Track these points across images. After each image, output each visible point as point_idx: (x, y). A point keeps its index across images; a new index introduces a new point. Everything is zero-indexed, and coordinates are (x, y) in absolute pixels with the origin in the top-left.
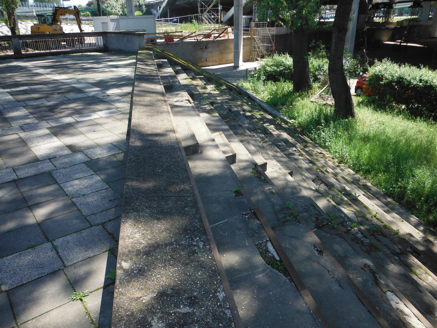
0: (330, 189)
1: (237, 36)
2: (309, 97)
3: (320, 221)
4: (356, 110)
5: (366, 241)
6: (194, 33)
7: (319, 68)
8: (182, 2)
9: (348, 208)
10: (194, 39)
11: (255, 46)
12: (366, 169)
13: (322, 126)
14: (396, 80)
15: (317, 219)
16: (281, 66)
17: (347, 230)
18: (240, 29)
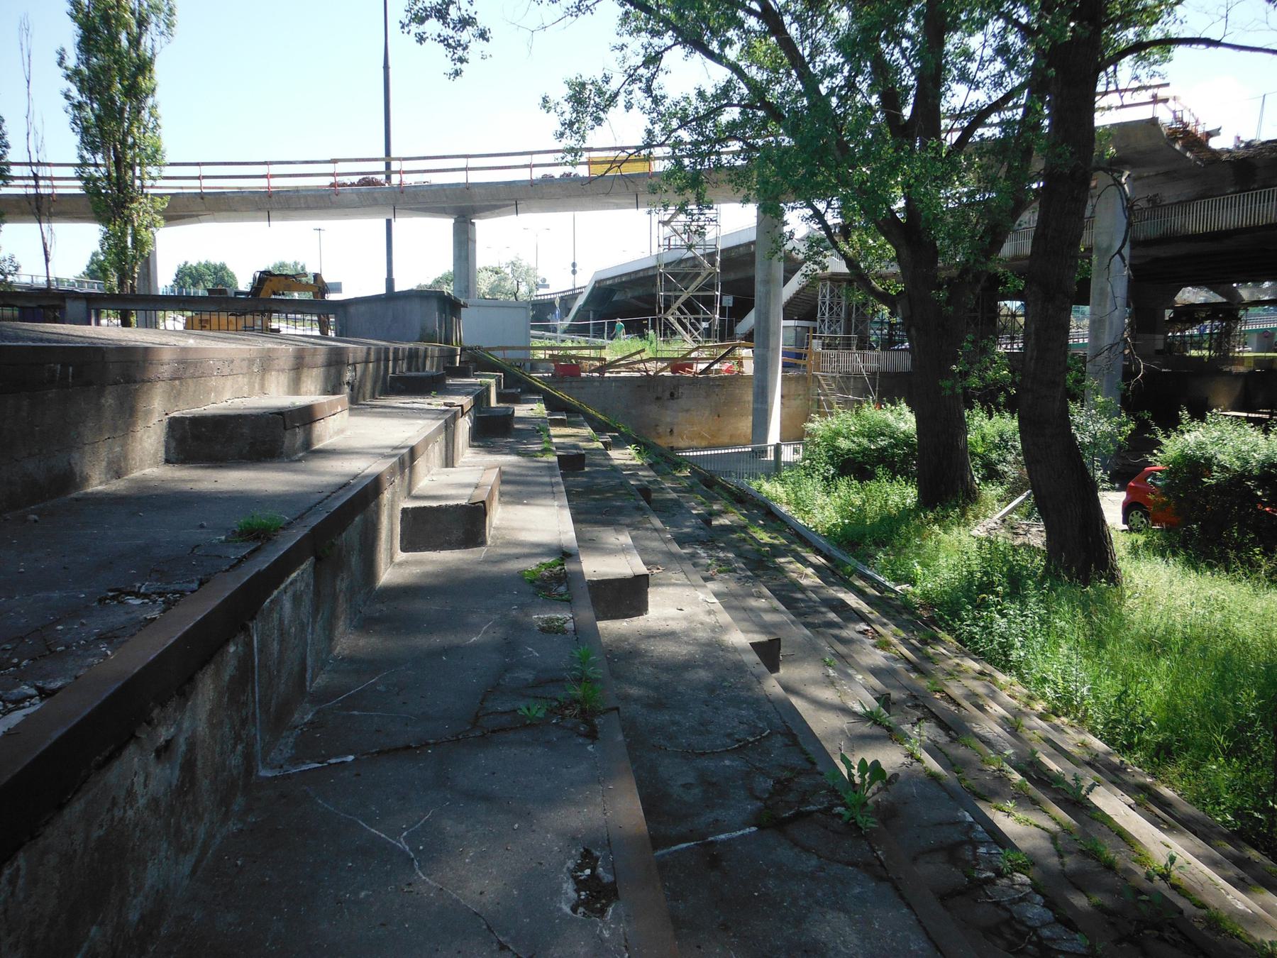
0: (953, 740)
1: (763, 365)
2: (967, 524)
3: (791, 797)
4: (1125, 564)
5: (1066, 946)
6: (639, 352)
7: (1003, 443)
8: (629, 295)
9: (1020, 815)
10: (639, 370)
11: (819, 400)
12: (1158, 744)
13: (997, 595)
14: (1256, 472)
15: (782, 787)
16: (883, 435)
17: (972, 879)
18: (772, 345)
